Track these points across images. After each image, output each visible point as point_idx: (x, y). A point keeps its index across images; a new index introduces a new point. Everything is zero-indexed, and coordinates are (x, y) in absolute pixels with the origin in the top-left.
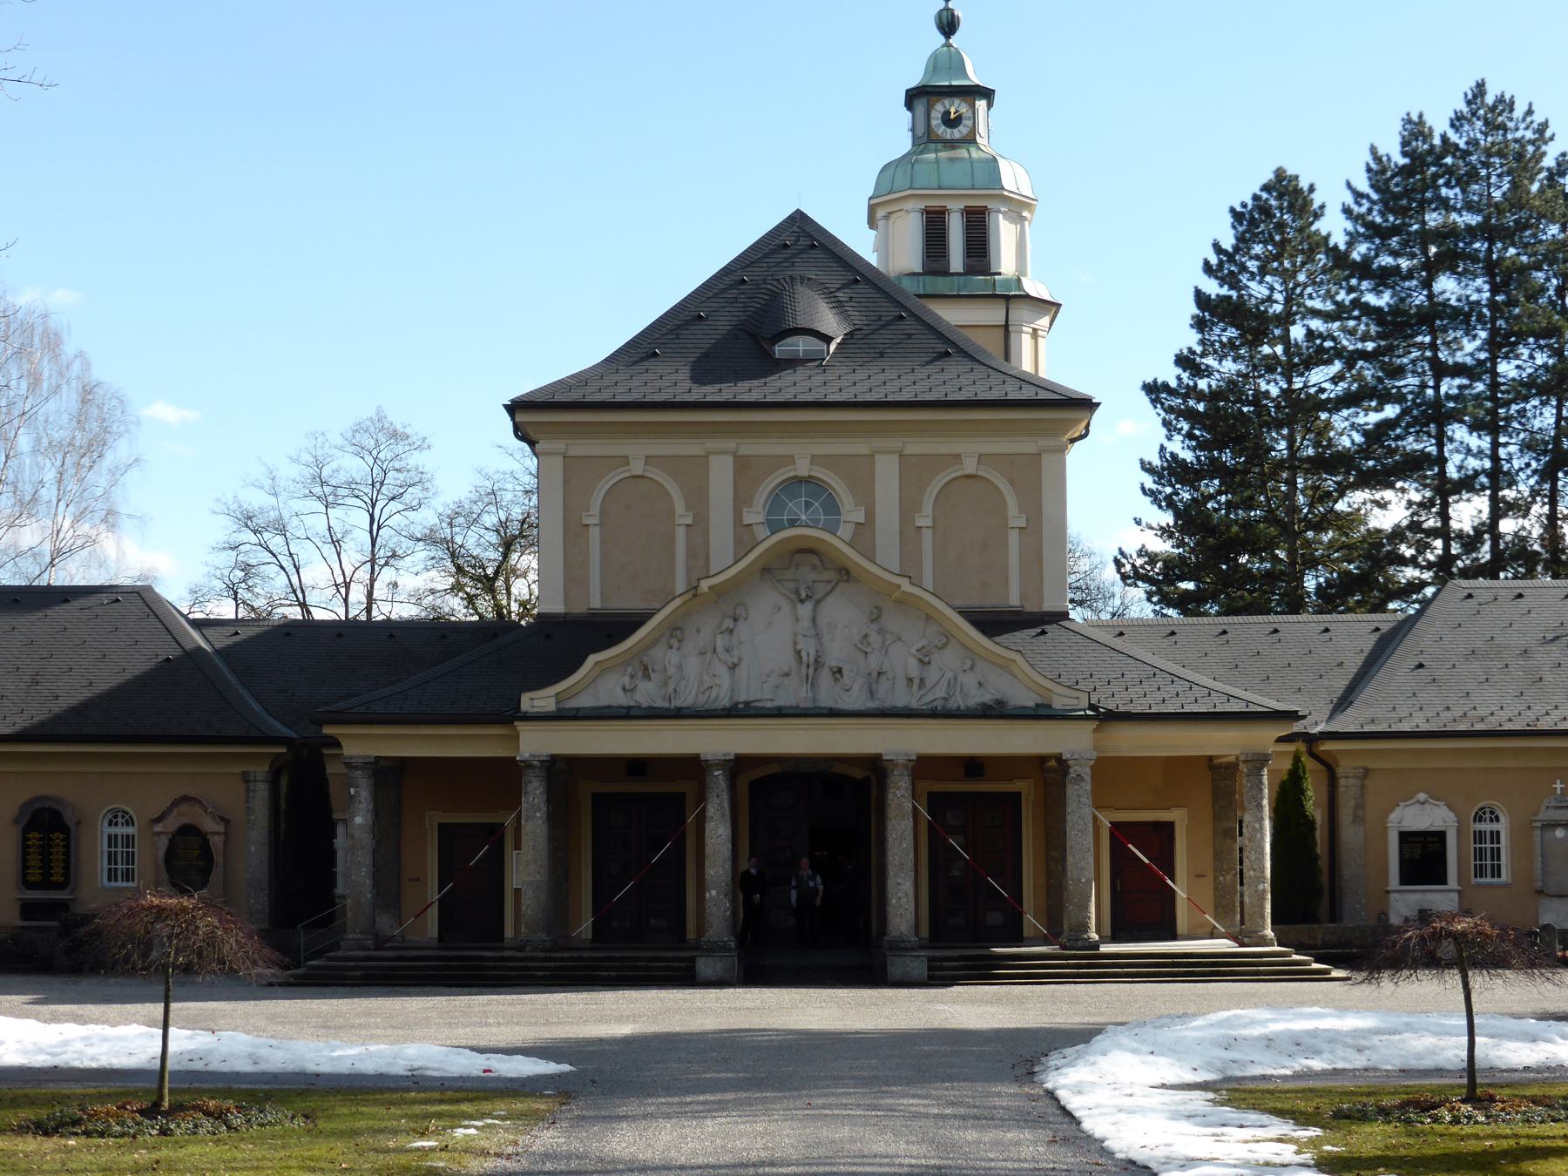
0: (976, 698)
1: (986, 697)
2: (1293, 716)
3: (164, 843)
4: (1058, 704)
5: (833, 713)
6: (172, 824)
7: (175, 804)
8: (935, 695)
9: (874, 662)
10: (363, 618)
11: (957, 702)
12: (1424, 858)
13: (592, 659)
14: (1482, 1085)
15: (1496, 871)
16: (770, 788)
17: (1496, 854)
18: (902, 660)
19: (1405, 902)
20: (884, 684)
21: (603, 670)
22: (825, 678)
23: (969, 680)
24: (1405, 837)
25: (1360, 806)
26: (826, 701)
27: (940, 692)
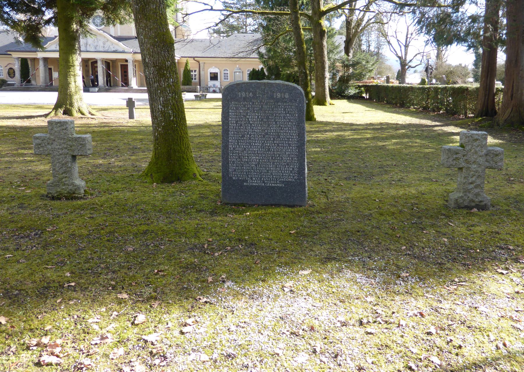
0: (113, 49)
1: (114, 50)
2: (514, 327)
3: (7, 70)
4: (126, 51)
5: (87, 51)
6: (8, 67)
7: (8, 64)
8: (106, 49)
9: (96, 44)
10: (395, 83)
11: (110, 50)
12: (214, 77)
13: (49, 43)
14: (217, 100)
15: (228, 79)
16: (109, 64)
17: (227, 76)
18: (101, 44)
19: (211, 83)
20: (98, 47)
21: (52, 44)
22: (88, 46)
23: (112, 47)
24: (211, 73)
25: (204, 68)
26: (88, 50)
27: (107, 48)
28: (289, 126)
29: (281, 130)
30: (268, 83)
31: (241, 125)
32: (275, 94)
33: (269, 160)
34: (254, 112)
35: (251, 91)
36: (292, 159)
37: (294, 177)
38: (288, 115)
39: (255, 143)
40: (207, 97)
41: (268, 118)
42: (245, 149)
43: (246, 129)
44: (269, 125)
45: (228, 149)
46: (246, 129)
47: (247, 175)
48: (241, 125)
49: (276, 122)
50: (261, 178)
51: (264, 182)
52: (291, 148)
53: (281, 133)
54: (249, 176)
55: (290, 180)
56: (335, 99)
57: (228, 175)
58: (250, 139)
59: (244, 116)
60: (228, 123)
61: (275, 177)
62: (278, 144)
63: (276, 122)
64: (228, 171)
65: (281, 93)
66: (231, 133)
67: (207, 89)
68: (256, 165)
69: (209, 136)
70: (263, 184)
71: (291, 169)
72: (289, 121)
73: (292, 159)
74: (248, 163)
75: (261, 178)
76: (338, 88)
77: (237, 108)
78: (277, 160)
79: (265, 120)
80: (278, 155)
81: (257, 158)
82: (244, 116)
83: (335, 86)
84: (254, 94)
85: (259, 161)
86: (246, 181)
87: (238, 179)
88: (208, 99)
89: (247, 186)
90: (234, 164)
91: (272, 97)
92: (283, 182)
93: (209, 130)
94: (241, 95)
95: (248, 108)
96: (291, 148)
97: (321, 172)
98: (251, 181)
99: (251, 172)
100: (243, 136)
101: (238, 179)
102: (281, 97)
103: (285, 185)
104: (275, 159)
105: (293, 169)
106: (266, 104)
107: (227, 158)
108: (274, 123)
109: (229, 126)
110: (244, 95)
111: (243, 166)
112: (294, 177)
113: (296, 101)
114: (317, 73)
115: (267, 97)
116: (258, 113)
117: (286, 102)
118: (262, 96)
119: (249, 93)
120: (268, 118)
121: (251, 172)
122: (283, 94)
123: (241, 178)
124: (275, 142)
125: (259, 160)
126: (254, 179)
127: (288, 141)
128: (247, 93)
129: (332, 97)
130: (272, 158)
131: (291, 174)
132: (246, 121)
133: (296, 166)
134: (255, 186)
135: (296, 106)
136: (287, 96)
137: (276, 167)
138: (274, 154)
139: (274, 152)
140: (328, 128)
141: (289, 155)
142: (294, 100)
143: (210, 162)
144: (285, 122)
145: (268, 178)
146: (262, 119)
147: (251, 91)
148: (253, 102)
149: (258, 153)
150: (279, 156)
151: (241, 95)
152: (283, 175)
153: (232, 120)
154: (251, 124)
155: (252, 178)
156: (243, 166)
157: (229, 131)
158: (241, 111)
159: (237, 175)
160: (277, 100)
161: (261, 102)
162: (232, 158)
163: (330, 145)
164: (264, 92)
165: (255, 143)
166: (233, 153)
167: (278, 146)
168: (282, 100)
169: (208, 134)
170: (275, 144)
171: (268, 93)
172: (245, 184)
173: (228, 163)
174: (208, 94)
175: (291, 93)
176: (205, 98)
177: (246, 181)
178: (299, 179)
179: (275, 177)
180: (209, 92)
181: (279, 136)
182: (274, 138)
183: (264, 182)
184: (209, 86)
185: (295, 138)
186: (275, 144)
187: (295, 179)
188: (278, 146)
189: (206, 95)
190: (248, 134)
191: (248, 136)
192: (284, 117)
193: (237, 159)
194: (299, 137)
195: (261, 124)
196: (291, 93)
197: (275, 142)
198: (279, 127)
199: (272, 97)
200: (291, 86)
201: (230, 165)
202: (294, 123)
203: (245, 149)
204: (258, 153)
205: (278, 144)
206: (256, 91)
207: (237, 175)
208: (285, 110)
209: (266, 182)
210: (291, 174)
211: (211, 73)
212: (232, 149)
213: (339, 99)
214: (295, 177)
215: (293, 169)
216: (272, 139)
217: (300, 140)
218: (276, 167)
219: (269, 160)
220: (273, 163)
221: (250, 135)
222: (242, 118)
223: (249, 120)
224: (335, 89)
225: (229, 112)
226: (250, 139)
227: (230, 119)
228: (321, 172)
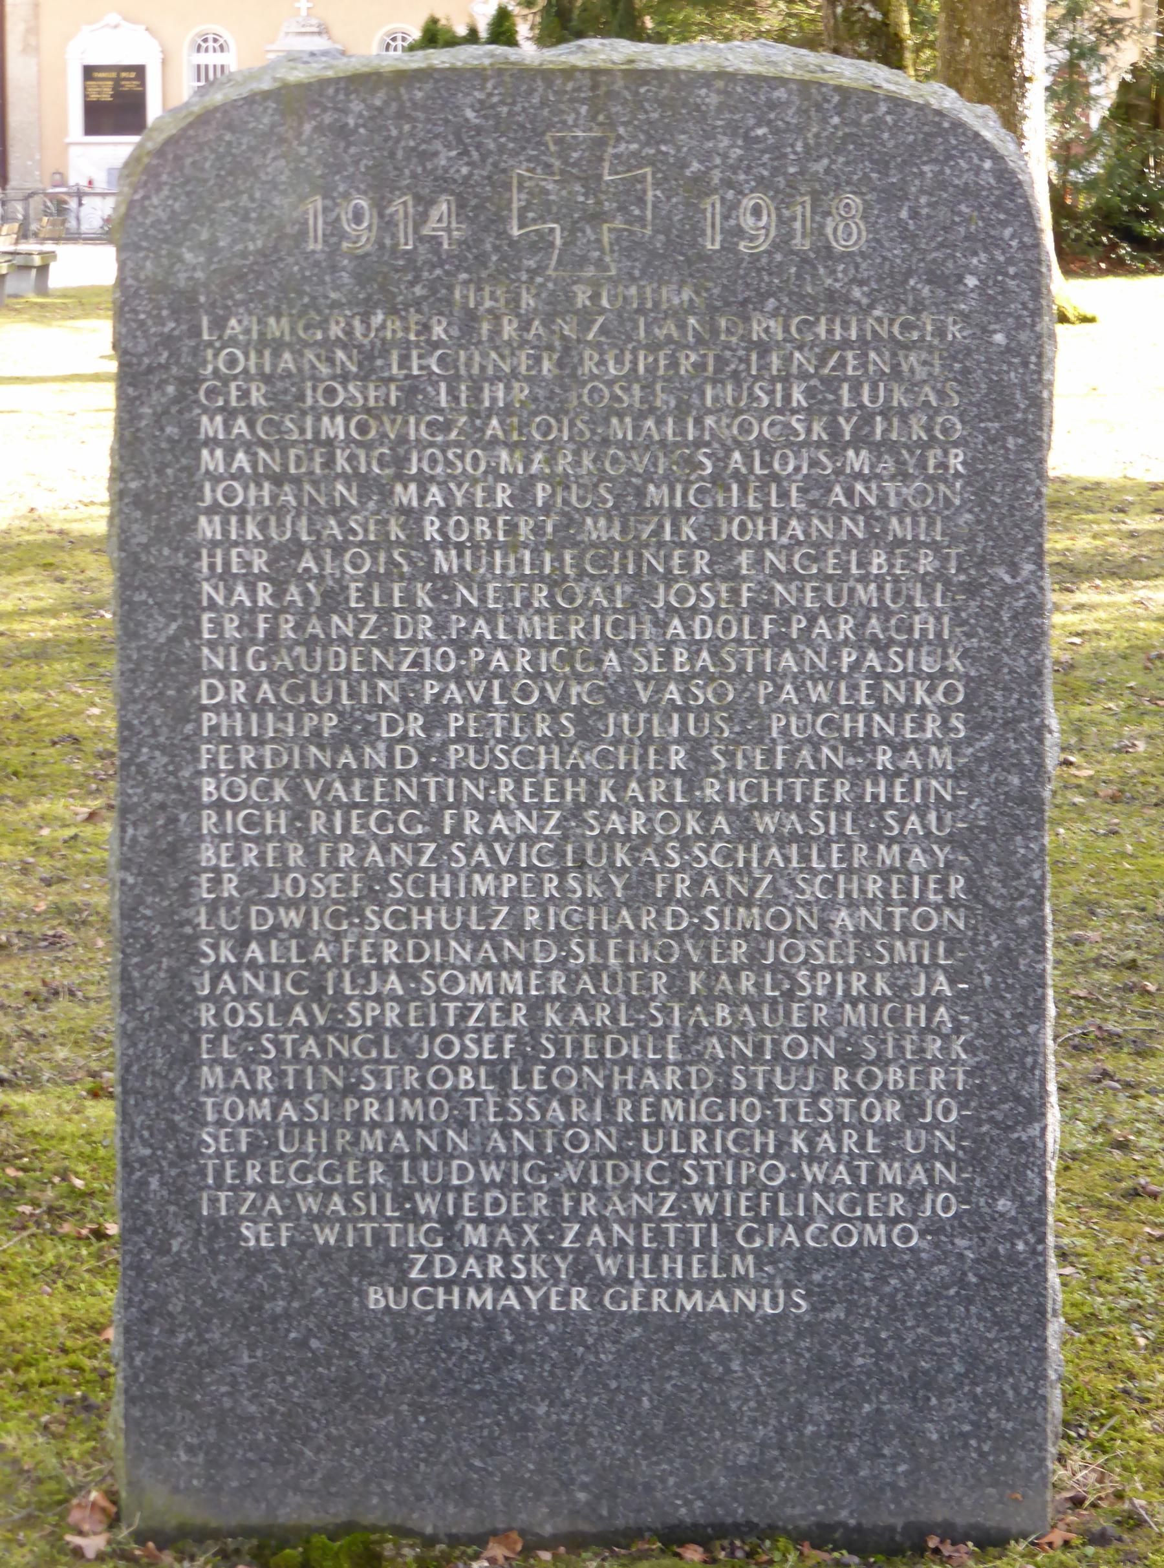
24: (89, 72)
25: (33, 30)
28: (866, 594)
29: (780, 641)
30: (638, 76)
31: (334, 601)
32: (713, 206)
33: (638, 1004)
34: (476, 437)
35: (443, 183)
36: (902, 991)
37: (915, 1196)
38: (858, 460)
39: (486, 810)
40: (57, 278)
41: (631, 503)
42: (375, 885)
43: (387, 643)
44: (645, 589)
45: (187, 887)
46: (387, 643)
47: (404, 1196)
48: (334, 601)
49: (723, 552)
50: (553, 1224)
51: (583, 1272)
52: (888, 855)
53: (777, 677)
54: (426, 1204)
55: (876, 1236)
56: (1086, 271)
57: (182, 1194)
58: (431, 758)
59: (365, 484)
60: (187, 580)
61: (704, 1204)
62: (742, 818)
63: (723, 552)
64: (190, 1153)
65: (784, 199)
66: (218, 697)
67: (61, 208)
68: (500, 1077)
69: (41, 652)
70: (578, 1300)
71: (893, 1110)
72: (875, 539)
73: (902, 991)
74: (409, 1054)
75: (553, 1224)
76: (1111, 171)
77: (286, 397)
78: (735, 1001)
79: (596, 529)
80: (739, 951)
81: (512, 982)
82: (365, 484)
83: (1089, 155)
84: (481, 209)
85: (537, 1028)
86: (392, 1265)
87: (303, 1245)
88: (65, 294)
89: (398, 1321)
90: (249, 1061)
91: (678, 253)
92: (803, 1262)
93: (47, 593)
94: (334, 230)
95: (412, 389)
96: (888, 855)
97: (1112, 1040)
98: (445, 1266)
99: (446, 1154)
100: (354, 733)
101: (303, 1245)
102: (783, 243)
103: (821, 1299)
104: (709, 998)
105: (912, 1106)
106: (618, 335)
107: (178, 1001)
108: (701, 562)
109: (191, 608)
110: (362, 236)
111: (352, 1090)
112: (915, 1196)
113: (947, 282)
114: (955, 39)
115: (629, 247)
116: (525, 447)
117: (836, 302)
118: (572, 231)
119: (426, 203)
120: (631, 503)
121: (446, 1154)
122: (802, 208)
123: (327, 1236)
124: (710, 791)
125: (535, 1007)
126: (476, 1236)
127: (856, 777)
128: (401, 206)
129: (1077, 257)
130: (677, 988)
131: (890, 1173)
132: (385, 542)
133: (949, 1065)
134: (490, 1320)
135: (954, 353)
136: (848, 229)
137: (725, 1092)
138: (699, 933)
139: (696, 905)
140: (1083, 542)
141: (865, 937)
142: (933, 279)
143: (31, 944)
144: (820, 546)
145: (637, 1221)
146: (570, 520)
147: (443, 183)
148: (470, 319)
149: (519, 933)
150: (755, 959)
151: (334, 230)
152: (793, 1186)
153: (229, 533)
154: (443, 585)
155: (449, 1228)
156: (352, 1090)
157: (196, 672)
158: (334, 428)
159: (288, 1195)
160: (739, 287)
161: (557, 305)
162: (234, 998)
163: (1133, 712)
164: (591, 183)
165: (486, 810)
166: (243, 940)
167: (746, 833)
168: (797, 280)
169: (34, 630)
170: (707, 812)
171: (631, 194)
172: (376, 1298)
173: (188, 1060)
174: (64, 251)
175: (891, 197)
176: (42, 288)
177: (392, 1265)
178: (975, 1224)
179: (704, 1204)
180: (75, 237)
181: (750, 721)
182: (697, 748)
183: (583, 1272)
184: (76, 178)
185: (939, 737)
186: (707, 812)
187: (934, 1228)
188: (746, 833)
189: (49, 256)
190: (408, 705)
191: (415, 725)
192: (817, 485)
193: (284, 1008)
194: (977, 727)
195: (555, 582)
196: (891, 197)
197: (710, 791)
198: (760, 607)
199: (678, 253)
200: (898, 103)
201: (211, 1077)
202: (926, 563)
203: (375, 885)
204: (519, 933)
205: (742, 818)
206: (500, 182)
207: (288, 1195)
208: (821, 401)
209: (608, 1266)
210: (890, 1173)
211: (89, 72)
212: (230, 887)
213: (1118, 267)
214: (936, 1205)
215: (912, 1106)
216: (677, 757)
217: (995, 755)
218: (725, 1092)
219: (638, 1004)
220: (692, 1039)
221: (435, 716)
222: (339, 510)
223: (416, 543)
224: (1092, 185)
225: (191, 442)
226: (431, 758)
227: (208, 528)
228: (1112, 1040)
